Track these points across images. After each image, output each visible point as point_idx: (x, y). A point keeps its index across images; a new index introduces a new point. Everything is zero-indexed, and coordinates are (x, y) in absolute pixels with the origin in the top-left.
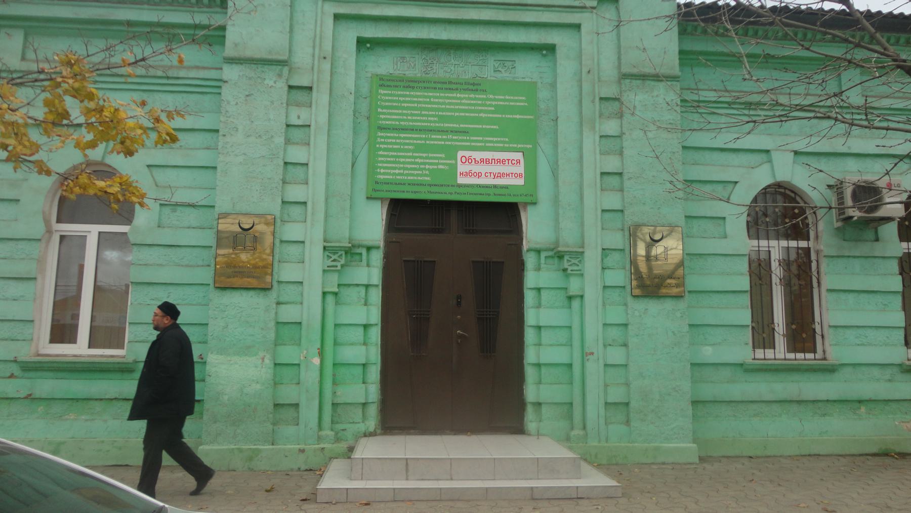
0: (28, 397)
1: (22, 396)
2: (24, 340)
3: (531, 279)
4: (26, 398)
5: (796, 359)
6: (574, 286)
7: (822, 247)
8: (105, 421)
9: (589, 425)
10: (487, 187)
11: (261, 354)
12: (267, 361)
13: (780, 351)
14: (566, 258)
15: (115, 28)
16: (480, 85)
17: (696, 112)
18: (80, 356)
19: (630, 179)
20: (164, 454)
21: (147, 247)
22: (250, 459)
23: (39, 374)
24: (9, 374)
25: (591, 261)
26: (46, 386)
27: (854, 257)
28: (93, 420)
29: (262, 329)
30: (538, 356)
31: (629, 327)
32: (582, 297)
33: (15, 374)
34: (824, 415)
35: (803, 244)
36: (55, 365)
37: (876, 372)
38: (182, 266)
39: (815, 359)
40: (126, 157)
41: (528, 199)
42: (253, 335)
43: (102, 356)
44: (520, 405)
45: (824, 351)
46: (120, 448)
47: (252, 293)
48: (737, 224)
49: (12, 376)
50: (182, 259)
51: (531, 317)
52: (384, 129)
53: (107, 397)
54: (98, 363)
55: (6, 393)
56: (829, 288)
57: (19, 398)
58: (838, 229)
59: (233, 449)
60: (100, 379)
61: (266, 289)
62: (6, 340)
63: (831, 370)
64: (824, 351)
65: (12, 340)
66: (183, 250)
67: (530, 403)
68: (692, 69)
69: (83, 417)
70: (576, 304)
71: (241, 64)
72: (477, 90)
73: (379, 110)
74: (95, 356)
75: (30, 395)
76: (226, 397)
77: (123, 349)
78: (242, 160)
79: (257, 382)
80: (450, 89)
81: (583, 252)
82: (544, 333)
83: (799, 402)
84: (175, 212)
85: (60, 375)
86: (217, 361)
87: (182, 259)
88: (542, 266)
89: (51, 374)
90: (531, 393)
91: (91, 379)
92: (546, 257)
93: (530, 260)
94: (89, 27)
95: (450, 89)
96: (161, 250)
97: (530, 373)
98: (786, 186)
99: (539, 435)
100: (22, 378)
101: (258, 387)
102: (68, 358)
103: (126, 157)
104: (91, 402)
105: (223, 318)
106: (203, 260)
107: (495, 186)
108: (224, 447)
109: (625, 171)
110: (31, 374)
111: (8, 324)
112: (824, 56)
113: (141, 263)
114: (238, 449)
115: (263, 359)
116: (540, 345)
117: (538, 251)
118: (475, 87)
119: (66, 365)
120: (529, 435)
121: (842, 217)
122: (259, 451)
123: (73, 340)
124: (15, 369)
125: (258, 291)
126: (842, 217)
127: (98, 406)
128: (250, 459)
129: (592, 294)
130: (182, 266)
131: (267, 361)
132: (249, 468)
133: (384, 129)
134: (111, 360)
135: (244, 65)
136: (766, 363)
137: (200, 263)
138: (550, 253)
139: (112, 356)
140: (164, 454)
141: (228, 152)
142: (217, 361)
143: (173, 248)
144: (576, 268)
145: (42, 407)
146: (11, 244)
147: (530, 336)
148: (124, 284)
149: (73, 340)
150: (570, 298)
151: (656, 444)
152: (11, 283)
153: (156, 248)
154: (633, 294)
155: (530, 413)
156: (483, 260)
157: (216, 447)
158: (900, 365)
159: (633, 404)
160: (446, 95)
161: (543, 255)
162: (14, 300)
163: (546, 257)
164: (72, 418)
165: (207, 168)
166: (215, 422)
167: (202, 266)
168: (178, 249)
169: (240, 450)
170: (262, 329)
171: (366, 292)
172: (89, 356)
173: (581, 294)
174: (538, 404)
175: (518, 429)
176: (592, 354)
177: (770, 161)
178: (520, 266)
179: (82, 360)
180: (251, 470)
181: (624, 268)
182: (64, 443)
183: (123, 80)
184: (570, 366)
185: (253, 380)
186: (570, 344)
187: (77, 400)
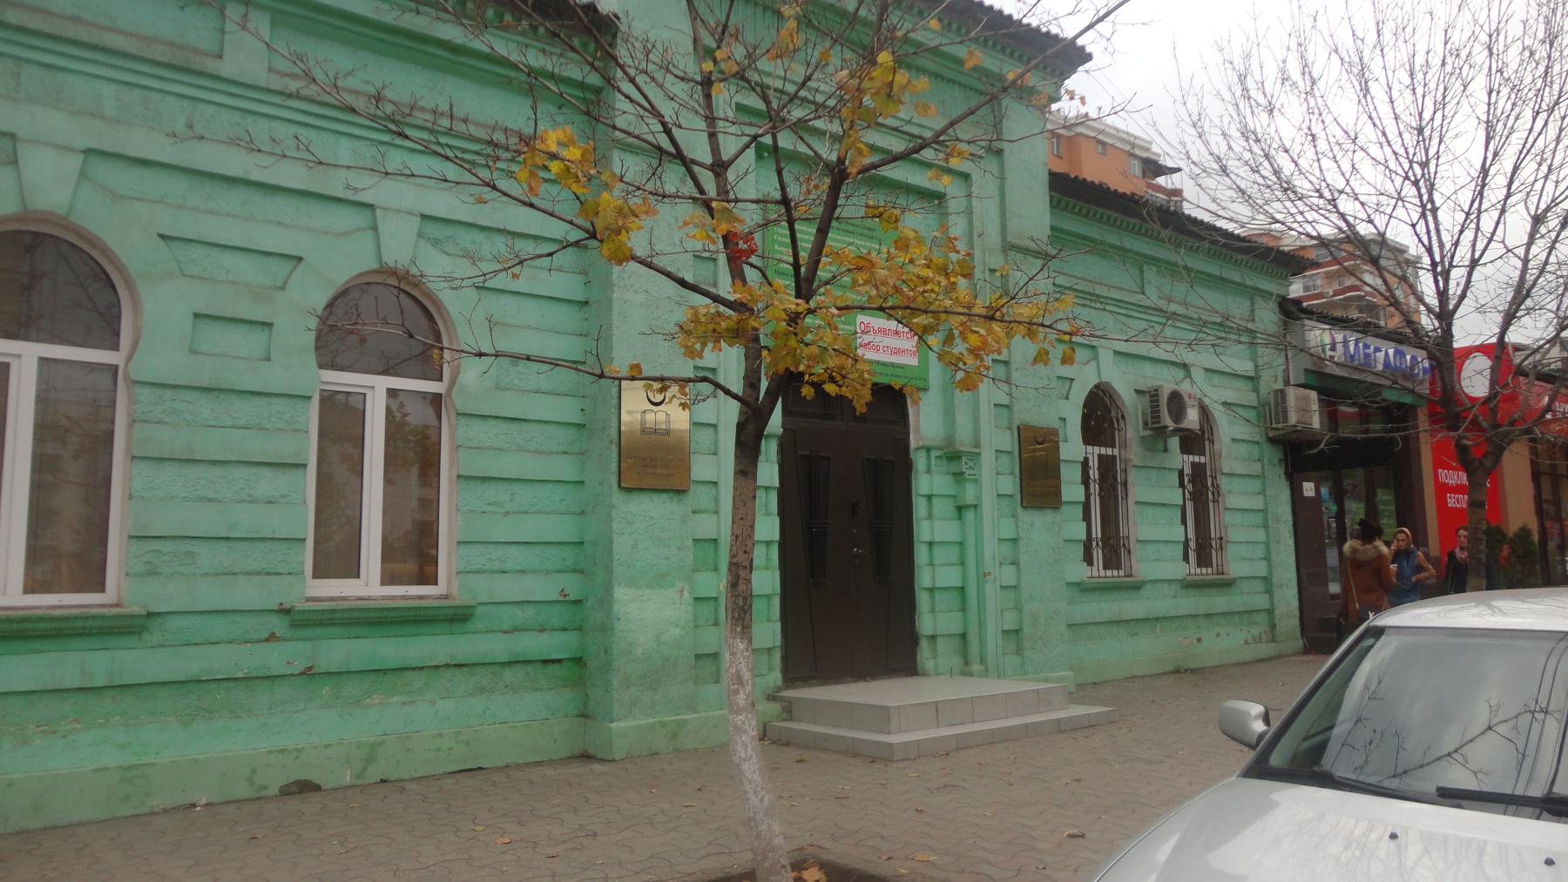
0: (308, 673)
1: (296, 671)
2: (290, 574)
4: (302, 674)
5: (1106, 577)
6: (970, 494)
7: (1132, 456)
8: (433, 702)
9: (990, 659)
10: (885, 364)
11: (679, 585)
12: (686, 595)
13: (1098, 569)
14: (964, 459)
15: (430, 49)
16: (874, 230)
17: (484, 166)
18: (369, 599)
19: (1017, 369)
21: (479, 421)
22: (675, 735)
23: (320, 631)
24: (266, 635)
26: (337, 651)
27: (1152, 468)
28: (413, 702)
29: (679, 548)
30: (933, 578)
31: (1021, 542)
33: (278, 635)
34: (1134, 635)
35: (1109, 451)
36: (356, 614)
37: (1166, 587)
38: (530, 451)
41: (920, 384)
42: (667, 558)
43: (404, 598)
44: (913, 639)
46: (468, 743)
47: (664, 497)
48: (296, 333)
49: (272, 638)
50: (530, 441)
52: (783, 274)
53: (433, 664)
54: (425, 608)
55: (269, 669)
56: (1138, 500)
57: (292, 675)
58: (1143, 438)
59: (654, 724)
60: (415, 635)
61: (680, 492)
62: (258, 573)
63: (1137, 587)
65: (268, 574)
66: (531, 426)
67: (926, 636)
69: (395, 700)
70: (969, 516)
71: (637, 154)
72: (872, 237)
73: (776, 247)
74: (393, 598)
75: (310, 668)
76: (640, 650)
78: (643, 300)
79: (677, 626)
80: (847, 231)
81: (979, 454)
82: (937, 550)
83: (1118, 622)
84: (517, 365)
85: (354, 631)
86: (626, 598)
87: (530, 441)
88: (933, 467)
89: (339, 631)
90: (926, 623)
91: (409, 636)
93: (919, 461)
94: (389, 38)
95: (847, 231)
96: (501, 424)
97: (923, 600)
99: (938, 674)
100: (291, 639)
101: (677, 632)
102: (349, 602)
104: (407, 674)
105: (631, 533)
106: (558, 444)
107: (893, 365)
108: (641, 722)
109: (1013, 360)
110: (308, 632)
111: (260, 546)
112: (813, 154)
113: (470, 444)
114: (660, 722)
115: (682, 592)
117: (928, 450)
118: (870, 234)
119: (376, 615)
120: (927, 675)
121: (1156, 426)
122: (684, 722)
123: (353, 571)
124: (279, 625)
125: (671, 494)
126: (1156, 426)
127: (416, 680)
128: (675, 735)
130: (530, 451)
131: (686, 595)
132: (675, 748)
133: (783, 274)
134: (403, 604)
135: (641, 156)
137: (555, 449)
139: (421, 598)
141: (625, 286)
142: (626, 598)
143: (517, 422)
144: (972, 472)
145: (327, 688)
146: (258, 401)
148: (1064, 508)
149: (353, 571)
151: (1045, 675)
152: (266, 472)
153: (494, 422)
154: (623, 485)
155: (924, 650)
156: (808, 453)
157: (631, 723)
158: (1180, 581)
159: (1027, 630)
160: (844, 238)
161: (934, 454)
162: (270, 502)
163: (936, 457)
164: (377, 701)
165: (559, 300)
166: (628, 687)
167: (557, 453)
168: (523, 424)
169: (663, 724)
170: (679, 548)
172: (384, 598)
173: (975, 503)
174: (933, 638)
175: (909, 668)
176: (990, 573)
177: (1096, 358)
178: (908, 466)
179: (372, 604)
180: (676, 750)
181: (1012, 473)
182: (381, 744)
183: (277, 100)
184: (962, 589)
185: (671, 623)
187: (385, 671)
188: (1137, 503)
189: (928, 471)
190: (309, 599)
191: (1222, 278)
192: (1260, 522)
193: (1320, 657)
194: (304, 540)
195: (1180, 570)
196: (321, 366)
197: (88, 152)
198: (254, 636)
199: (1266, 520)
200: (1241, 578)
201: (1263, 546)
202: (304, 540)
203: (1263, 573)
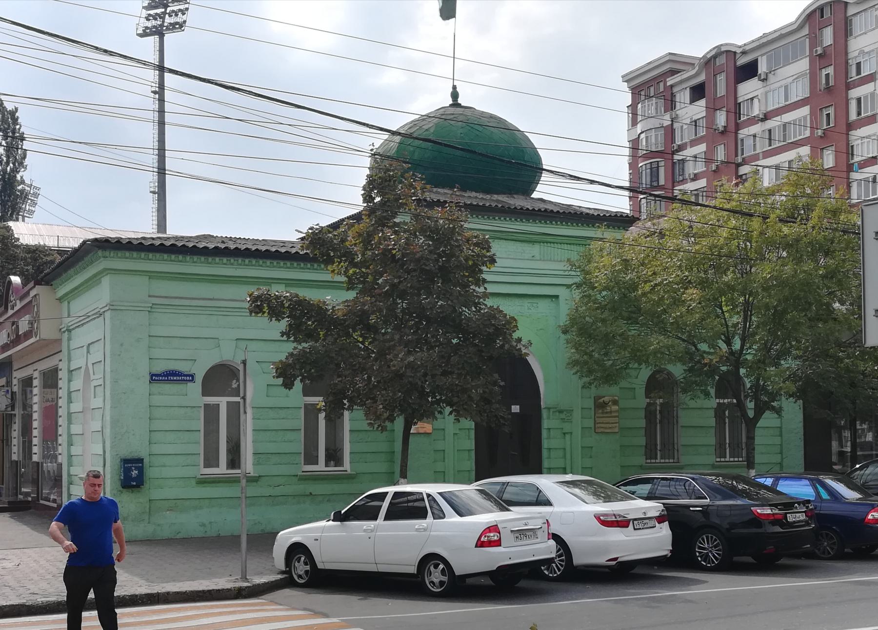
3: (546, 424)
6: (567, 427)
20: (92, 590)
25: (577, 415)
32: (571, 433)
39: (674, 462)
40: (280, 333)
45: (678, 458)
51: (545, 444)
63: (681, 468)
64: (678, 458)
68: (455, 95)
70: (568, 436)
77: (227, 469)
88: (551, 416)
89: (226, 484)
92: (553, 412)
93: (545, 414)
98: (551, 262)
103: (280, 333)
116: (550, 458)
129: (578, 432)
136: (238, 615)
138: (555, 410)
140: (92, 590)
147: (545, 453)
150: (564, 434)
161: (552, 410)
171: (469, 433)
186: (565, 457)
188: (682, 426)
189: (548, 418)
190: (303, 472)
191: (419, 433)
192: (778, 433)
193: (590, 498)
194: (300, 430)
195: (712, 459)
196: (304, 396)
197: (237, 339)
198: (267, 478)
199: (781, 432)
200: (686, 465)
201: (779, 446)
202: (300, 430)
203: (779, 461)
